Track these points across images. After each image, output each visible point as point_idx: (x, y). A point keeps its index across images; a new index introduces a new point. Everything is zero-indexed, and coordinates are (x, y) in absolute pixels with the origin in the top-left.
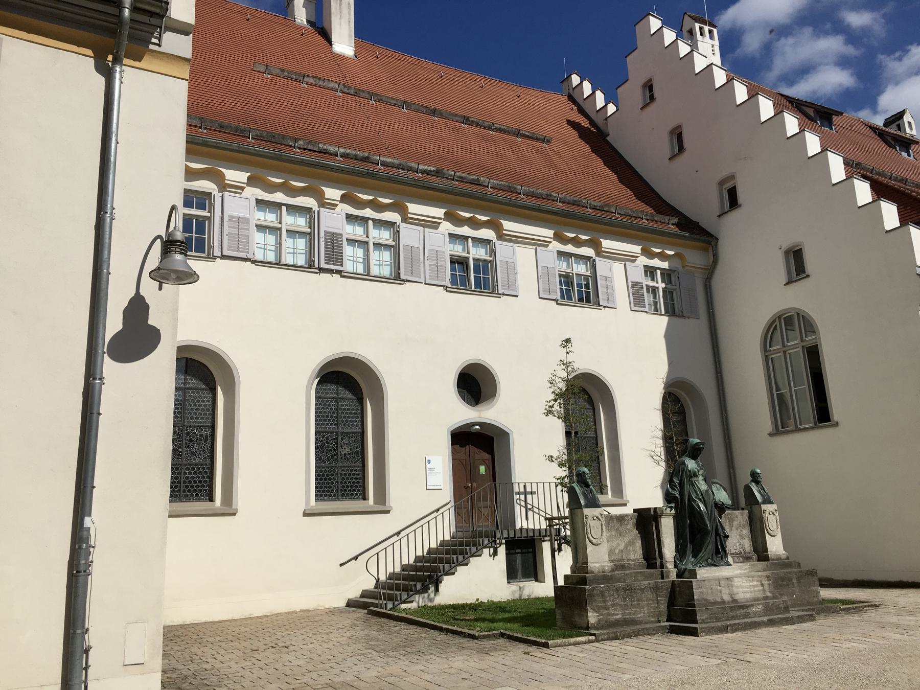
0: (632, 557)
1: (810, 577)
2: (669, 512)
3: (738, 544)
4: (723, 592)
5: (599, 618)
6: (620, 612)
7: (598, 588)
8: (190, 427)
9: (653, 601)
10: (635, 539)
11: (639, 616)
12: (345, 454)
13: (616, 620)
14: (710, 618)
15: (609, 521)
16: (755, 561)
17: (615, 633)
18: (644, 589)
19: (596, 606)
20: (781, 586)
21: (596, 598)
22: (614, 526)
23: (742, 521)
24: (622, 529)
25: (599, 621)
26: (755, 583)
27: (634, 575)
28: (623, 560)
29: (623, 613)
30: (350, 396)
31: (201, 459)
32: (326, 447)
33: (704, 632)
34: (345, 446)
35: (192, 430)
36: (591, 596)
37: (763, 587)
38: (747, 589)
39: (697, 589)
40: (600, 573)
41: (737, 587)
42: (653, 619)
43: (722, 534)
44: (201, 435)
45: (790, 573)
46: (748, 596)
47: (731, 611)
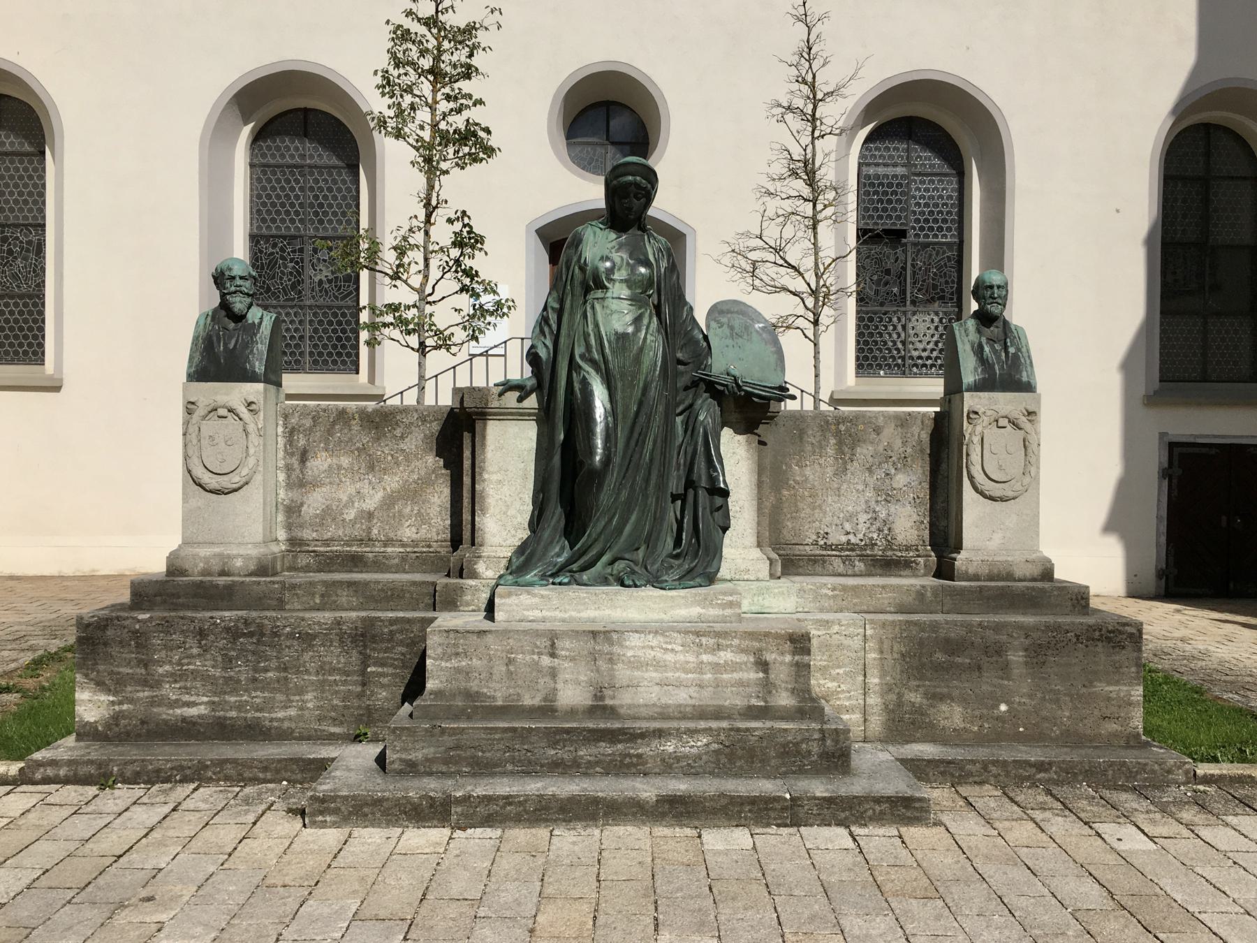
0: (408, 533)
1: (1099, 649)
2: (514, 404)
3: (863, 517)
4: (561, 677)
5: (117, 708)
6: (205, 699)
7: (127, 623)
8: (9, 226)
9: (347, 674)
10: (426, 482)
11: (281, 715)
12: (321, 282)
13: (184, 719)
14: (447, 761)
15: (334, 424)
16: (925, 575)
17: (100, 764)
18: (314, 637)
19: (111, 673)
20: (938, 668)
21: (114, 650)
22: (351, 440)
23: (898, 443)
24: (383, 450)
25: (116, 717)
26: (726, 656)
27: (320, 589)
28: (368, 540)
29: (214, 703)
30: (335, 161)
31: (30, 287)
32: (279, 267)
33: (336, 811)
34: (321, 266)
35: (12, 233)
36: (93, 644)
37: (766, 671)
38: (683, 676)
39: (445, 657)
40: (210, 574)
41: (638, 664)
42: (333, 730)
43: (704, 483)
44: (30, 243)
45: (998, 628)
46: (682, 697)
47: (553, 745)
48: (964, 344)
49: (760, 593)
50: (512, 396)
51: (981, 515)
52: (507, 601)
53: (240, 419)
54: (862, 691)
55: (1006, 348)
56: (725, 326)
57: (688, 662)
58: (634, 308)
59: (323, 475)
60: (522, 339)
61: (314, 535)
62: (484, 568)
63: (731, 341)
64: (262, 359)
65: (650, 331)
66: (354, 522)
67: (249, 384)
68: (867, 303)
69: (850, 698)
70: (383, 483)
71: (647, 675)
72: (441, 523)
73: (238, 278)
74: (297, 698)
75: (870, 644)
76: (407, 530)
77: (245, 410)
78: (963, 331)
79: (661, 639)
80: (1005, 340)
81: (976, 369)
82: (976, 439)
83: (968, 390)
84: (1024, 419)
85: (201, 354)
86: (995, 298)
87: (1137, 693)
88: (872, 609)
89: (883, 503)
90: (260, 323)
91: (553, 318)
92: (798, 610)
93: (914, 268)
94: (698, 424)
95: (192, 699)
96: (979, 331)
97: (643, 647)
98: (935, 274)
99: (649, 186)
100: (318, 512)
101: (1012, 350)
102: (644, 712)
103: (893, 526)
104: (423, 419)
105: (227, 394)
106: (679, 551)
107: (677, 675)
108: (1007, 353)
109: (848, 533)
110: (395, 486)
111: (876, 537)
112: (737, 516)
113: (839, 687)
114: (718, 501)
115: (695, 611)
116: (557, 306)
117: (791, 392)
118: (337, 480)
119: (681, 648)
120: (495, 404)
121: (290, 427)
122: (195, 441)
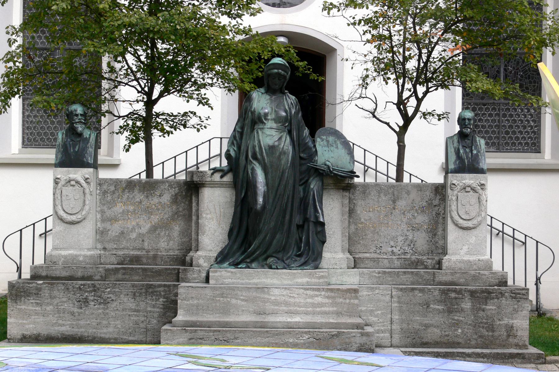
3: (400, 238)
43: (312, 219)
48: (451, 148)
49: (342, 274)
50: (217, 177)
51: (457, 237)
52: (217, 274)
53: (82, 187)
54: (390, 323)
55: (471, 151)
56: (325, 141)
57: (300, 302)
58: (277, 133)
59: (120, 215)
60: (221, 138)
61: (115, 246)
62: (203, 261)
63: (327, 148)
64: (91, 156)
65: (286, 144)
66: (135, 240)
67: (86, 169)
68: (472, 97)
69: (384, 326)
70: (150, 220)
71: (281, 308)
72: (180, 240)
73: (79, 115)
74: (113, 323)
75: (395, 299)
76: (163, 244)
77: (84, 182)
78: (451, 142)
79: (288, 291)
80: (472, 146)
81: (455, 161)
82: (454, 198)
83: (451, 173)
84: (479, 187)
85: (62, 154)
86: (466, 125)
87: (526, 324)
88: (398, 284)
89: (411, 231)
90: (90, 137)
91: (237, 136)
92: (361, 284)
93: (506, 71)
94: (310, 190)
95: (64, 322)
96: (459, 142)
97: (280, 295)
98: (522, 76)
99: (285, 74)
100: (117, 234)
101: (475, 152)
102: (279, 325)
103: (416, 243)
104: (171, 186)
105: (75, 174)
106: (300, 253)
107: (295, 308)
108: (472, 153)
109: (392, 247)
110: (156, 220)
111: (407, 249)
112: (331, 236)
113: (379, 320)
114: (319, 229)
115: (305, 280)
116: (239, 130)
117: (357, 174)
118: (127, 218)
119: (297, 296)
120: (209, 179)
121: (103, 190)
122: (59, 198)
